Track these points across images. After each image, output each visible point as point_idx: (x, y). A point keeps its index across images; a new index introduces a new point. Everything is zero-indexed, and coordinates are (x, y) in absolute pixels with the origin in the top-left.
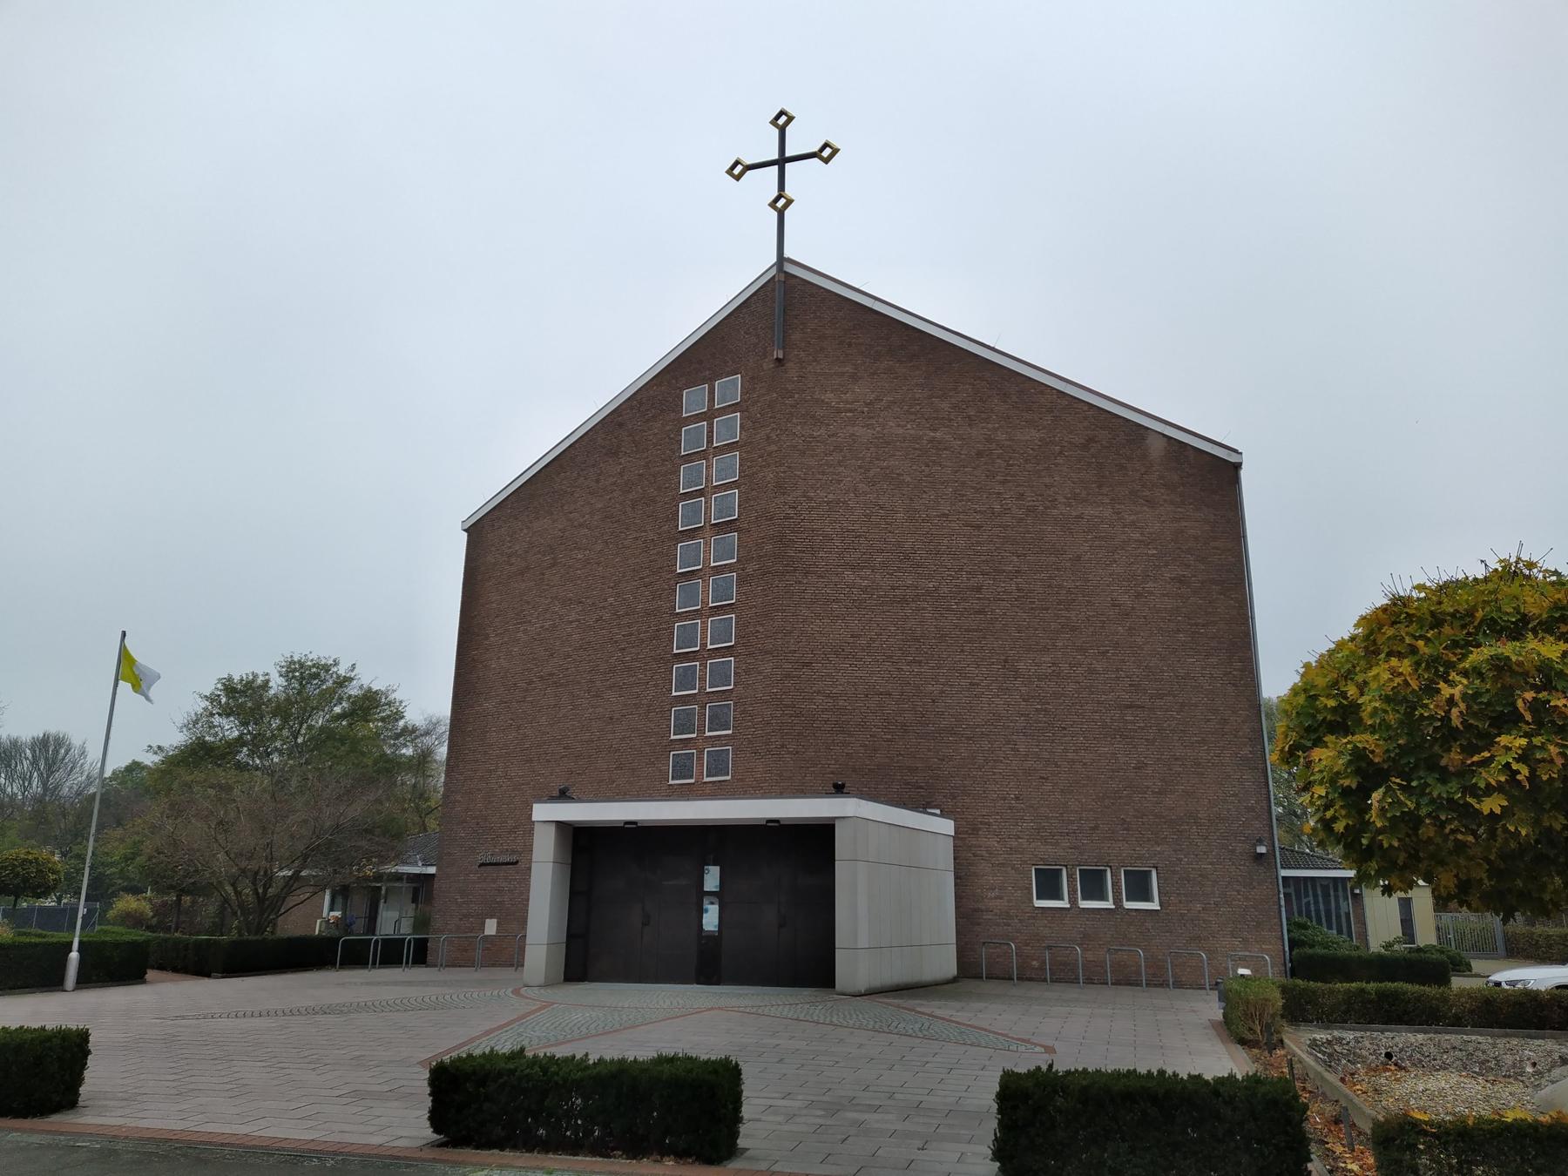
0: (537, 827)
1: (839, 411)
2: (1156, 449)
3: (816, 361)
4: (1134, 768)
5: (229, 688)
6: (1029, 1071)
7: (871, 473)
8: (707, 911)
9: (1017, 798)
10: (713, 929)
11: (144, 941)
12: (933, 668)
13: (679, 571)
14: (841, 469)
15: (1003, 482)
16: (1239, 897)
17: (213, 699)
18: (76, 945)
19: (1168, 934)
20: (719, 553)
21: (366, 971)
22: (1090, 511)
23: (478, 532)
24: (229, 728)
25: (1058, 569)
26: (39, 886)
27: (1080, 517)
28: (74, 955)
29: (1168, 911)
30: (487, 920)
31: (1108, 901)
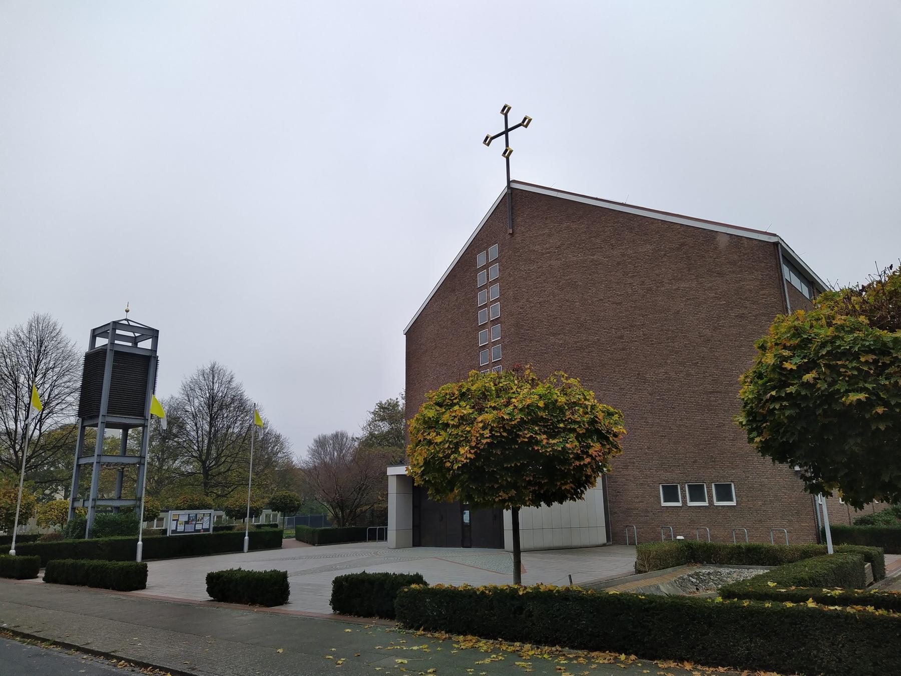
0: (390, 479)
1: (543, 254)
2: (723, 242)
3: (530, 230)
4: (717, 427)
5: (381, 407)
6: (265, 571)
7: (560, 284)
8: (465, 513)
9: (648, 448)
10: (467, 522)
11: (279, 531)
12: (599, 382)
13: (480, 346)
14: (545, 284)
15: (632, 277)
16: (786, 496)
17: (374, 413)
18: (247, 534)
20: (494, 334)
21: (376, 543)
22: (683, 285)
23: (413, 334)
24: (385, 427)
25: (666, 321)
26: (292, 507)
27: (678, 289)
28: (247, 538)
29: (741, 506)
31: (706, 502)
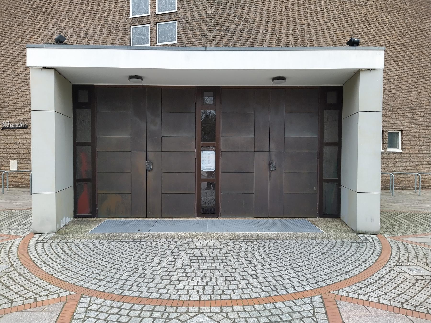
0: (34, 75)
19: (404, 164)
30: (11, 161)
